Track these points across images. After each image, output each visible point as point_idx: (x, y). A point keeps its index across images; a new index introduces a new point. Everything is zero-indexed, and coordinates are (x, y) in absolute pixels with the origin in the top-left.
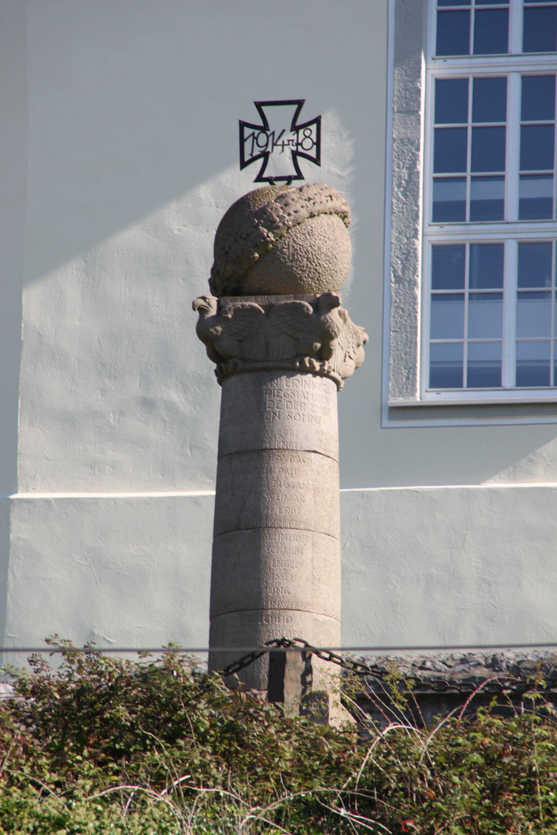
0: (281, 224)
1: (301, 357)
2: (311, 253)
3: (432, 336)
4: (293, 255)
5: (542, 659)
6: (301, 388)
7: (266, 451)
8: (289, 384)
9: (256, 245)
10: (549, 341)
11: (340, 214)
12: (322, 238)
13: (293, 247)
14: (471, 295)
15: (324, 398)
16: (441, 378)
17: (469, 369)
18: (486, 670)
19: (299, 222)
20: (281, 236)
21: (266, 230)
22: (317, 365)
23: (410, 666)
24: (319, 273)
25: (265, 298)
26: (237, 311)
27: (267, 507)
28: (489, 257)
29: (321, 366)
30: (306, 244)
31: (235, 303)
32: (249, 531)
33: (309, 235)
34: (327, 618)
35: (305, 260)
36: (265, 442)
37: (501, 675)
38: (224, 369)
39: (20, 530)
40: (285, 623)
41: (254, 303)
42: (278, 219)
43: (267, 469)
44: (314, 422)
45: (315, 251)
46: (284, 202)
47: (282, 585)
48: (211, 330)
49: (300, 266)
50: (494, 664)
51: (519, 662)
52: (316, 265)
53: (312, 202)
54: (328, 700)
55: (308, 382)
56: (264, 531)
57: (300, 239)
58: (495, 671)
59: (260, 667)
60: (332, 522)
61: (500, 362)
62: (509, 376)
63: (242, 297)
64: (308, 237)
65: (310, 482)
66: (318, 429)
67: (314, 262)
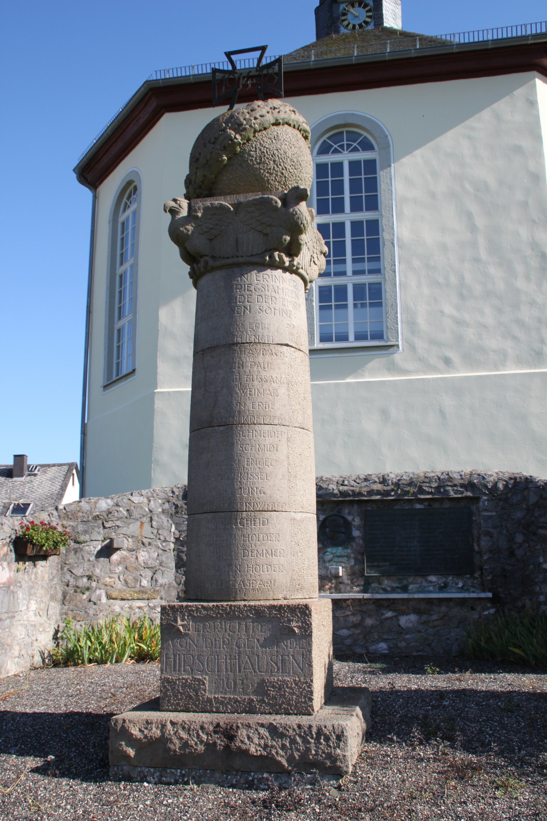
0: (247, 126)
1: (270, 251)
2: (278, 155)
3: (320, 322)
4: (260, 157)
5: (411, 478)
6: (271, 283)
7: (237, 346)
8: (259, 279)
9: (225, 147)
10: (367, 322)
11: (302, 132)
12: (287, 144)
13: (260, 150)
14: (335, 305)
15: (294, 293)
16: (323, 339)
17: (335, 336)
18: (380, 485)
19: (265, 126)
20: (248, 140)
21: (233, 132)
22: (287, 260)
23: (335, 483)
24: (285, 177)
25: (233, 197)
26: (206, 209)
27: (240, 403)
28: (341, 291)
29: (290, 261)
30: (273, 147)
31: (204, 203)
32: (222, 428)
33: (275, 140)
34: (304, 515)
35: (272, 162)
36: (237, 336)
37: (389, 488)
38: (196, 269)
39: (158, 404)
40: (262, 526)
41: (226, 202)
42: (245, 122)
43: (239, 364)
44: (285, 315)
45: (281, 155)
46: (251, 108)
47: (257, 485)
48: (181, 229)
49: (267, 169)
50: (384, 481)
51: (399, 480)
52: (283, 169)
53: (277, 111)
54: (310, 614)
55: (278, 277)
56: (237, 428)
57: (267, 142)
58: (385, 485)
59: (236, 575)
60: (305, 415)
61: (348, 332)
62: (351, 337)
63: (212, 198)
64: (274, 141)
65: (283, 376)
66: (289, 323)
67: (280, 165)
